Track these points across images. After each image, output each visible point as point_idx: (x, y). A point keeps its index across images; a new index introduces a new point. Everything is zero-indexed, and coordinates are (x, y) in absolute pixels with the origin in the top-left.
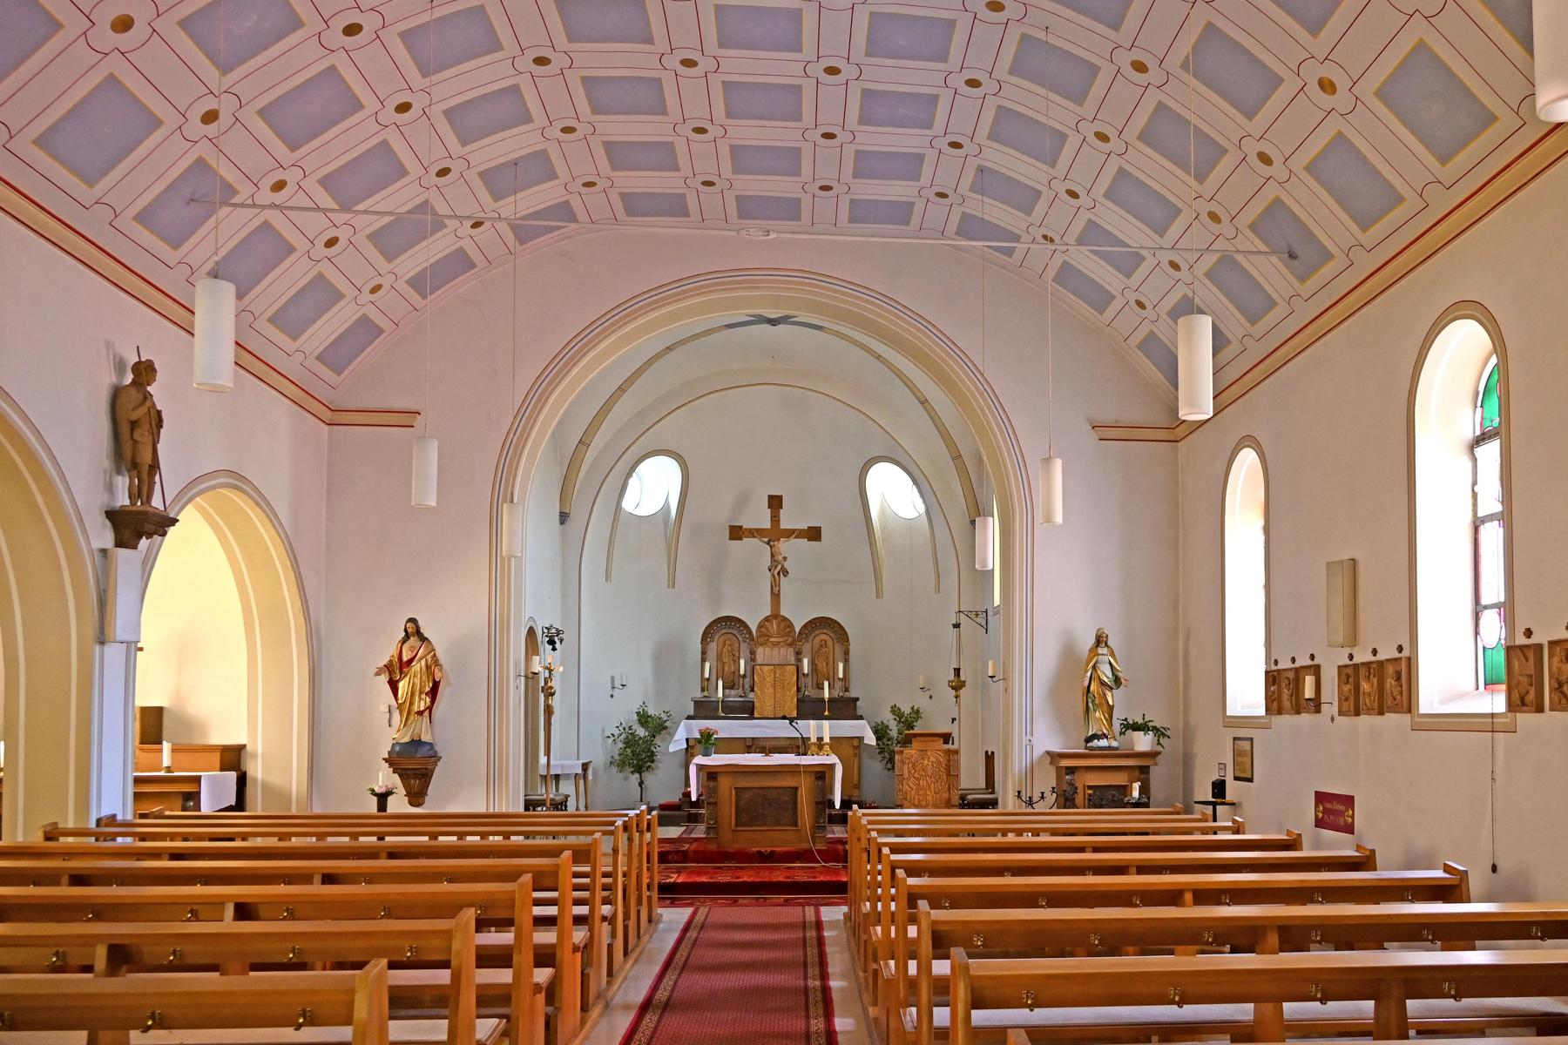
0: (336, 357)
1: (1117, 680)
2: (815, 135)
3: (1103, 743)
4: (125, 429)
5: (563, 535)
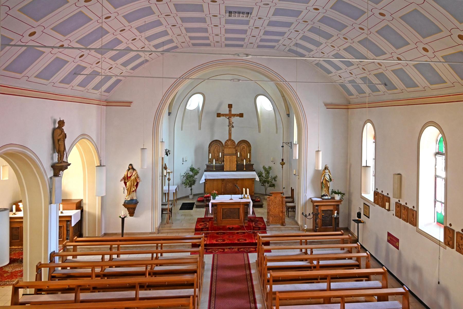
1: (331, 179)
3: (326, 197)
4: (56, 141)
5: (169, 119)
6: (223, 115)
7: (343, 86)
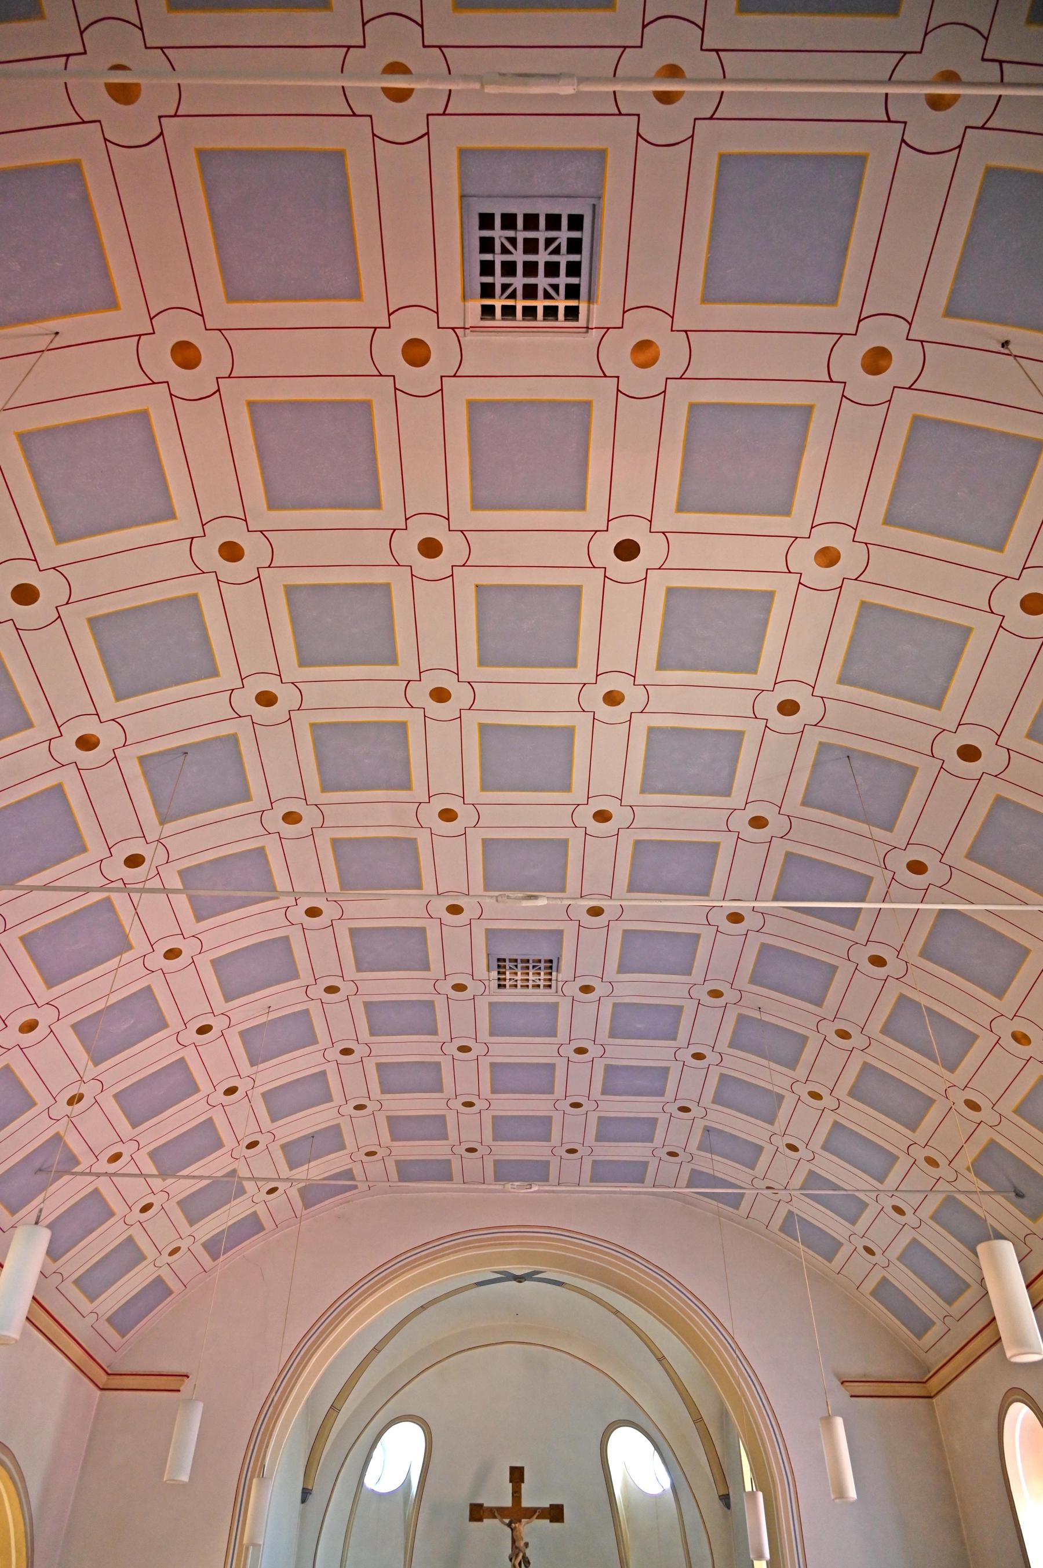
0: (122, 1321)
2: (565, 1105)
5: (303, 1516)
7: (884, 1290)
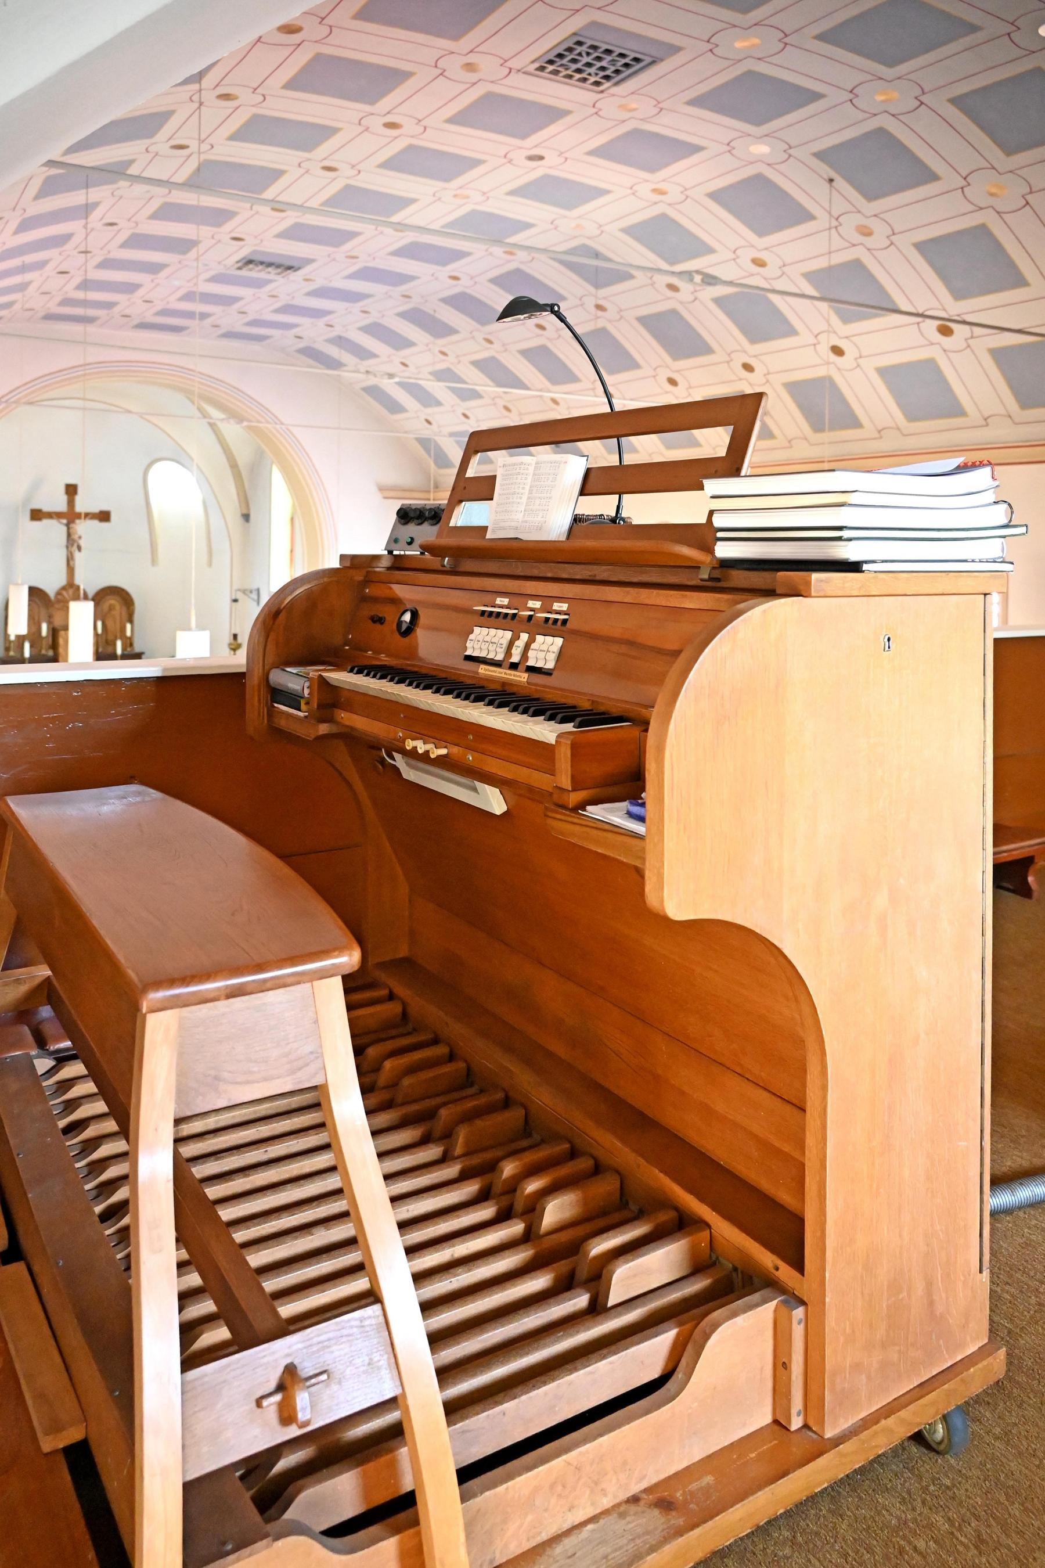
6: (50, 515)
